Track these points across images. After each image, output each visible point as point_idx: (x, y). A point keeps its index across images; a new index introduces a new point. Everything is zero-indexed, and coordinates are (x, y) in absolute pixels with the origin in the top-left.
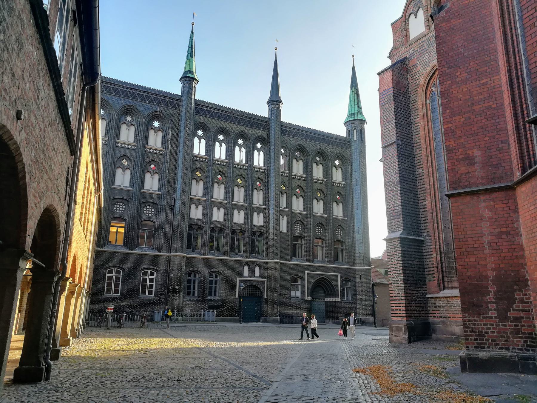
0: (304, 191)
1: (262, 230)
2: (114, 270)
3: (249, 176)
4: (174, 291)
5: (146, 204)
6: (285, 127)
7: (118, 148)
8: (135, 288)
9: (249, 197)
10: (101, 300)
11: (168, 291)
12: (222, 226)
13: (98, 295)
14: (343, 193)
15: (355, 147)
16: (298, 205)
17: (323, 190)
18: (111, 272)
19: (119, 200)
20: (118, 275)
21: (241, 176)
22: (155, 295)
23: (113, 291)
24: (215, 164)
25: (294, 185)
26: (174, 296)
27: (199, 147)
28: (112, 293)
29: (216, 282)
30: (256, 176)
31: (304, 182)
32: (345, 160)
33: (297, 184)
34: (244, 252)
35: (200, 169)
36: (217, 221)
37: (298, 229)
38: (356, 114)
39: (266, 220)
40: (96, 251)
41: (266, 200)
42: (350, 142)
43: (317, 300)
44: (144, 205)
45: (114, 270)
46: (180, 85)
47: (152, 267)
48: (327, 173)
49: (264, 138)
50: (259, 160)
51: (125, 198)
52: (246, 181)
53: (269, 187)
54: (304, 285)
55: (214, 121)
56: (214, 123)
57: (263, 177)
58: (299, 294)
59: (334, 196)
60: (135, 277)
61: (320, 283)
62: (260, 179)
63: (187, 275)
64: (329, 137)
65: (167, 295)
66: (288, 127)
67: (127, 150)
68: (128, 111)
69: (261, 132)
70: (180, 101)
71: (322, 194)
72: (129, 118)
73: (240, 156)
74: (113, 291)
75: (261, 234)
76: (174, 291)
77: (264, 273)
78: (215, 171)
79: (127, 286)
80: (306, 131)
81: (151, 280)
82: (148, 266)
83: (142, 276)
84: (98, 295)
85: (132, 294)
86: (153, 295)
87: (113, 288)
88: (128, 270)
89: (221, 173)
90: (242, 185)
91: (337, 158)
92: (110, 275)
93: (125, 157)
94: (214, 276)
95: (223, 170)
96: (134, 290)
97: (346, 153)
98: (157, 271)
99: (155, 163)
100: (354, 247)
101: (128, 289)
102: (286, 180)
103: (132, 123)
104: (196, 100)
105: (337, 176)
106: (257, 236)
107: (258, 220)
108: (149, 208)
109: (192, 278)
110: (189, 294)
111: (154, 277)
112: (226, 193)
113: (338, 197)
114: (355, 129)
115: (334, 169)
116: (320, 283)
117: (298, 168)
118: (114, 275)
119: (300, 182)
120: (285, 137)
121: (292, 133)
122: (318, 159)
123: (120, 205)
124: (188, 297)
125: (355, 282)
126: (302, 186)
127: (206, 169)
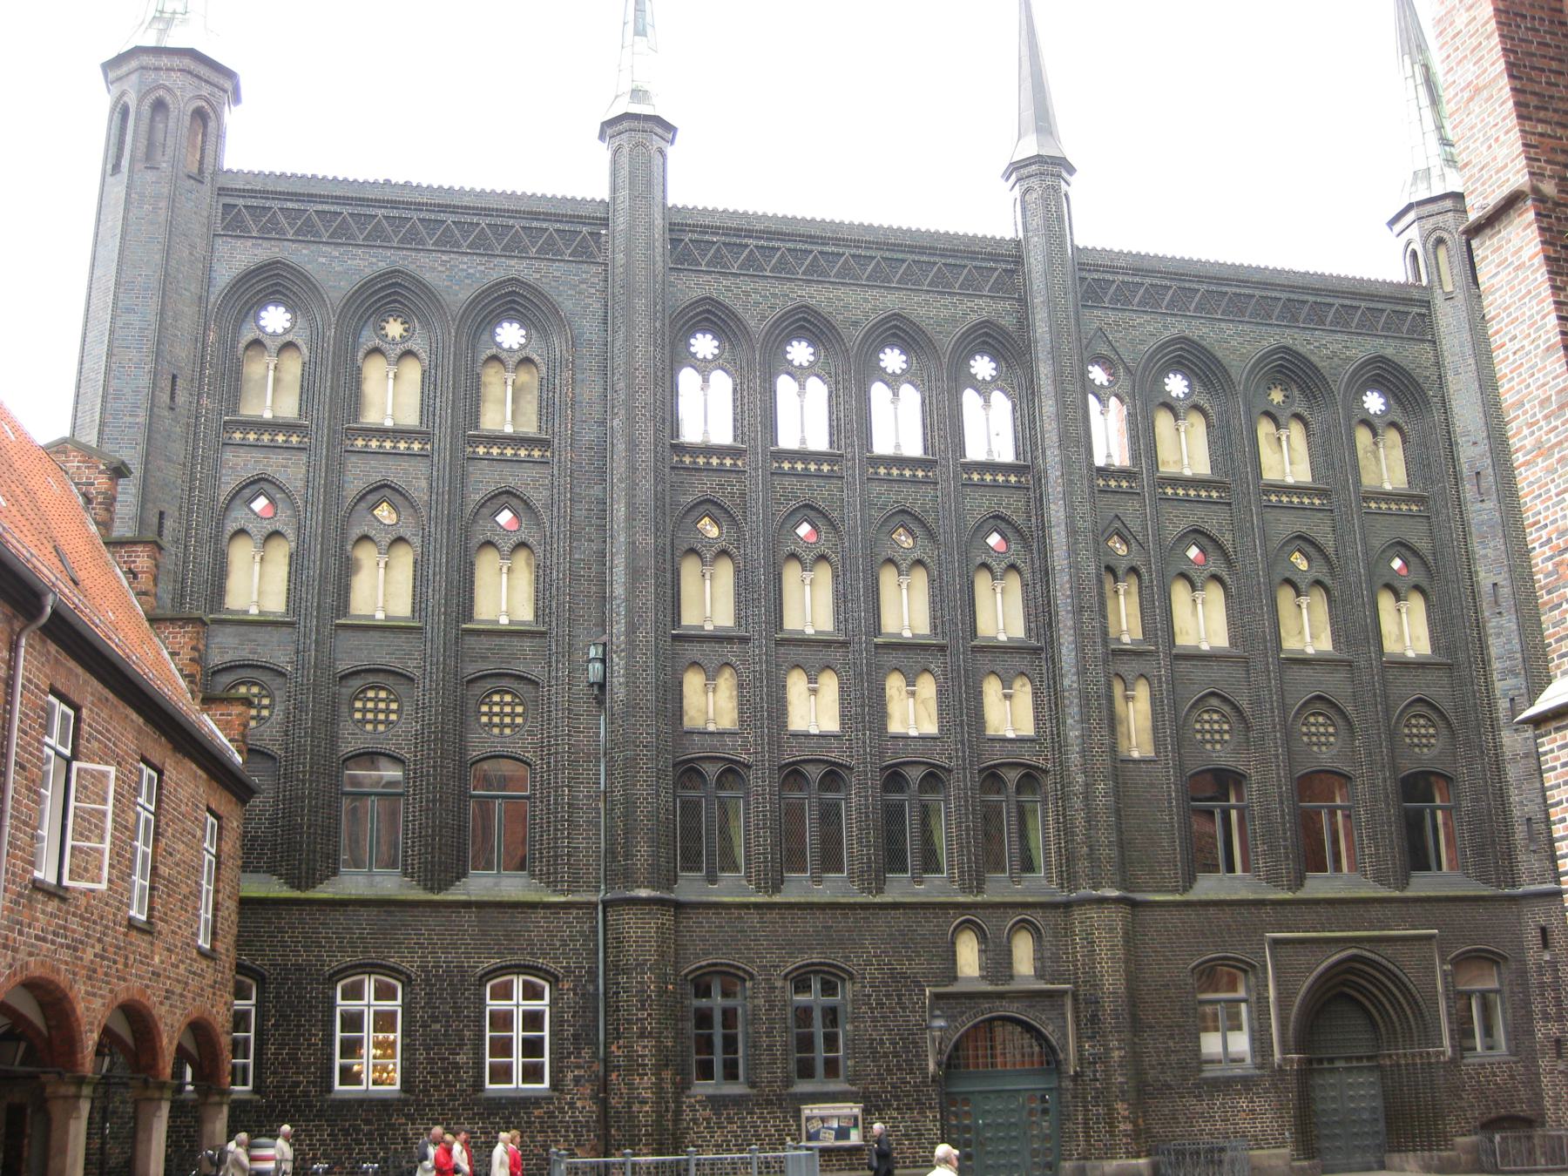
0: (1225, 554)
1: (1027, 759)
2: (518, 984)
3: (938, 515)
4: (633, 1066)
5: (489, 685)
6: (1096, 268)
7: (354, 458)
8: (461, 1059)
9: (953, 606)
10: (320, 1114)
11: (608, 1066)
12: (834, 756)
13: (306, 1094)
14: (1423, 545)
15: (1449, 320)
16: (1203, 622)
17: (1320, 540)
18: (354, 992)
19: (371, 679)
20: (534, 1005)
21: (906, 517)
22: (555, 1085)
23: (517, 1072)
24: (780, 473)
25: (1173, 530)
26: (631, 1086)
27: (706, 409)
28: (517, 1082)
29: (831, 1015)
30: (979, 505)
31: (1223, 514)
32: (1414, 395)
33: (1183, 527)
34: (951, 867)
35: (710, 506)
36: (807, 736)
37: (1218, 744)
38: (1435, 172)
39: (1049, 705)
40: (245, 903)
41: (1040, 611)
42: (1427, 304)
43: (1340, 1064)
44: (478, 689)
45: (518, 984)
46: (602, 154)
47: (529, 960)
48: (1333, 456)
49: (1001, 329)
50: (989, 430)
51: (397, 665)
52: (931, 535)
53: (1044, 553)
54: (1262, 1001)
55: (761, 284)
56: (756, 300)
57: (1012, 506)
58: (1240, 1043)
59: (1374, 564)
60: (455, 1007)
61: (1344, 983)
62: (998, 521)
63: (690, 989)
64: (1316, 291)
65: (603, 1087)
66: (1113, 269)
67: (391, 461)
68: (389, 295)
69: (982, 308)
70: (605, 222)
71: (1319, 561)
72: (394, 329)
73: (897, 424)
74: (517, 1072)
75: (1031, 778)
76: (633, 1066)
77: (1056, 959)
78: (783, 511)
79: (428, 1049)
80: (1200, 278)
81: (533, 1020)
82: (510, 959)
83: (492, 1005)
84: (306, 1094)
85: (449, 1084)
86: (546, 1084)
87: (517, 1060)
88: (427, 981)
89: (809, 511)
90: (917, 555)
91: (1377, 383)
92: (353, 1005)
93: (387, 492)
94: (816, 985)
95: (821, 495)
96: (457, 1066)
97: (1410, 355)
98: (554, 979)
99: (514, 502)
100: (1502, 795)
101: (431, 1061)
102: (1130, 510)
103: (409, 345)
104: (1076, 249)
105: (1386, 467)
106: (1012, 787)
107: (1009, 713)
108: (502, 704)
109: (717, 1001)
110: (706, 1072)
111: (543, 1005)
112: (841, 600)
113: (1397, 564)
114: (1440, 241)
115: (1363, 437)
116: (1344, 983)
117: (1187, 450)
118: (518, 1004)
119: (1200, 511)
120: (1096, 318)
121: (1105, 291)
122: (1277, 396)
123: (377, 700)
124: (702, 1089)
125: (1523, 962)
126: (1212, 526)
127: (749, 502)
